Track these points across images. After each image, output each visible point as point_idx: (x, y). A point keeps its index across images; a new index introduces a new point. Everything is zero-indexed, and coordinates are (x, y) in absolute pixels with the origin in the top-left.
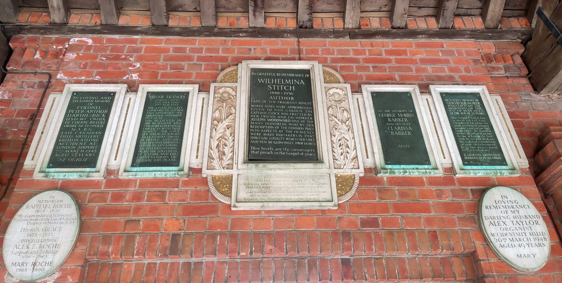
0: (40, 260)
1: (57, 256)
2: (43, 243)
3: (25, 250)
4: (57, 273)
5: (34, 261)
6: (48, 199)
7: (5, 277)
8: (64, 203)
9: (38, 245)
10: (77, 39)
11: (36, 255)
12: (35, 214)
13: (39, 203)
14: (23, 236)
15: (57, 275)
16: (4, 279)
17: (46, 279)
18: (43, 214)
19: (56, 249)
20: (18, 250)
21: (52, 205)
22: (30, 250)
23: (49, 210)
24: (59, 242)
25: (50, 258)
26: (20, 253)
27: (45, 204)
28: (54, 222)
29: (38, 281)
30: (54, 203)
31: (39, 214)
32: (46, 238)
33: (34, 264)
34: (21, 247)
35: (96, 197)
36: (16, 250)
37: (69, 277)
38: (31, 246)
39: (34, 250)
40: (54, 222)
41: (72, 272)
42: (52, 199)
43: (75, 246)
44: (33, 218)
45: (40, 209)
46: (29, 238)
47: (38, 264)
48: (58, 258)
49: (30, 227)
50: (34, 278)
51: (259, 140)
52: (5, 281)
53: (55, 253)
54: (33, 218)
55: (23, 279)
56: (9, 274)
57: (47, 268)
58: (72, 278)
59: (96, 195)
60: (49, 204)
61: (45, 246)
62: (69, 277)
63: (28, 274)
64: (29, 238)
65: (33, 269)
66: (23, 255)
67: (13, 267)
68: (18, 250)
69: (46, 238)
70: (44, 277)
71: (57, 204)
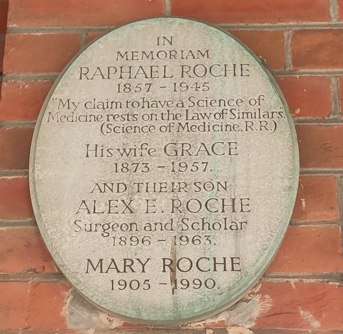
0: (189, 252)
1: (249, 237)
2: (182, 196)
3: (123, 218)
4: (257, 298)
5: (168, 255)
6: (150, 46)
7: (65, 311)
8: (215, 60)
9: (164, 201)
10: (277, 70)
11: (169, 235)
12: (122, 97)
13: (122, 61)
14: (97, 170)
15: (258, 307)
16: (63, 320)
17: (222, 318)
18: (148, 96)
19: (240, 217)
20: (96, 218)
21: (173, 67)
22: (142, 219)
23: (168, 83)
24: (240, 193)
25: (224, 246)
26: (106, 229)
27: (146, 63)
28: (199, 123)
29: (194, 325)
30: (178, 62)
31: (136, 97)
32: (187, 176)
33: (172, 265)
34: (102, 207)
35: (321, 46)
36: (86, 219)
37: (306, 314)
38: (139, 203)
39: (153, 218)
40: (199, 123)
41: (315, 300)
42: (167, 48)
43: (298, 212)
44: (117, 111)
45: (134, 83)
46: (123, 177)
47: (184, 265)
48: (258, 242)
49: (116, 141)
50: (186, 313)
51: (289, 274)
52: (70, 326)
53: (238, 228)
54: (117, 111)
55: (145, 316)
56: (80, 299)
57: (225, 279)
58: (318, 316)
59: (317, 39)
60: (161, 62)
61: (194, 206)
62: (306, 314)
63: (157, 299)
64: (123, 177)
65: (174, 281)
66: (119, 233)
67: (95, 274)
68: (96, 218)
69: (187, 176)
70: (216, 312)
71: (191, 62)
